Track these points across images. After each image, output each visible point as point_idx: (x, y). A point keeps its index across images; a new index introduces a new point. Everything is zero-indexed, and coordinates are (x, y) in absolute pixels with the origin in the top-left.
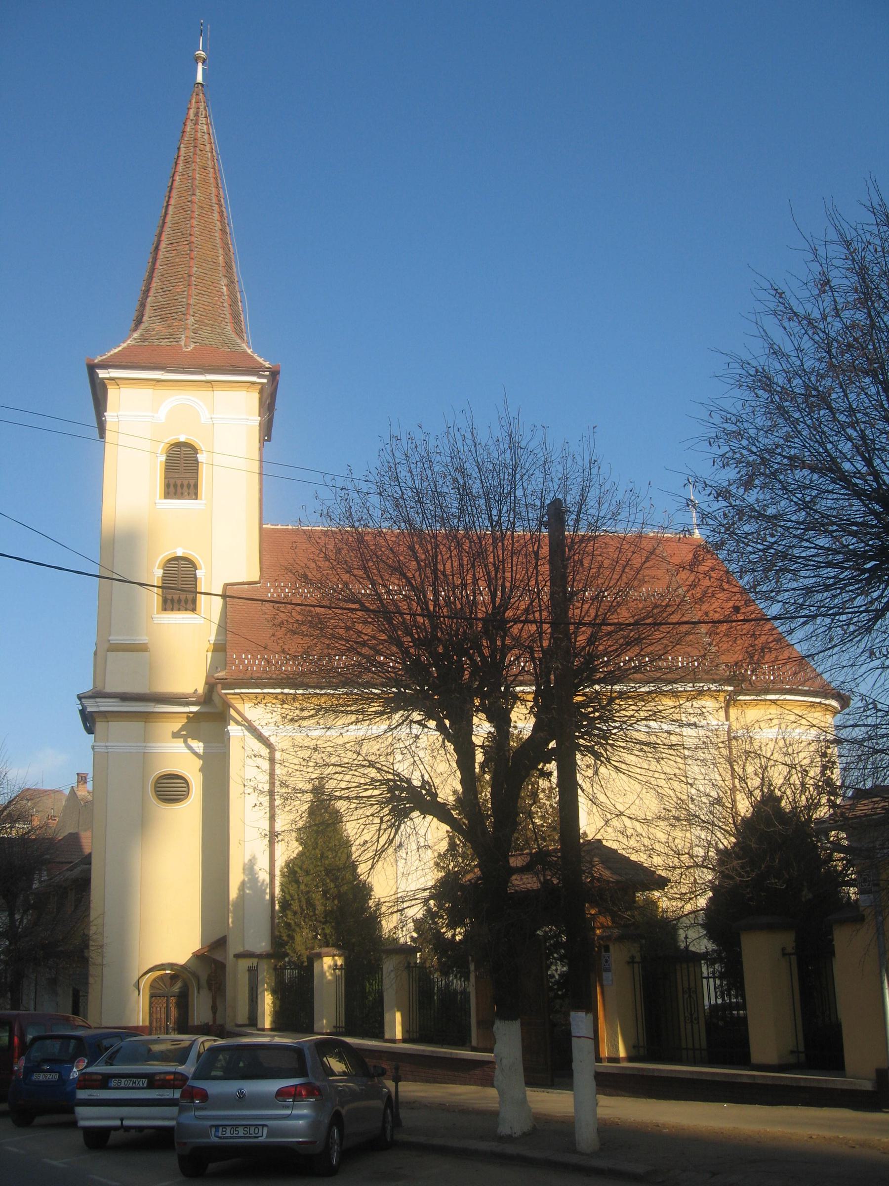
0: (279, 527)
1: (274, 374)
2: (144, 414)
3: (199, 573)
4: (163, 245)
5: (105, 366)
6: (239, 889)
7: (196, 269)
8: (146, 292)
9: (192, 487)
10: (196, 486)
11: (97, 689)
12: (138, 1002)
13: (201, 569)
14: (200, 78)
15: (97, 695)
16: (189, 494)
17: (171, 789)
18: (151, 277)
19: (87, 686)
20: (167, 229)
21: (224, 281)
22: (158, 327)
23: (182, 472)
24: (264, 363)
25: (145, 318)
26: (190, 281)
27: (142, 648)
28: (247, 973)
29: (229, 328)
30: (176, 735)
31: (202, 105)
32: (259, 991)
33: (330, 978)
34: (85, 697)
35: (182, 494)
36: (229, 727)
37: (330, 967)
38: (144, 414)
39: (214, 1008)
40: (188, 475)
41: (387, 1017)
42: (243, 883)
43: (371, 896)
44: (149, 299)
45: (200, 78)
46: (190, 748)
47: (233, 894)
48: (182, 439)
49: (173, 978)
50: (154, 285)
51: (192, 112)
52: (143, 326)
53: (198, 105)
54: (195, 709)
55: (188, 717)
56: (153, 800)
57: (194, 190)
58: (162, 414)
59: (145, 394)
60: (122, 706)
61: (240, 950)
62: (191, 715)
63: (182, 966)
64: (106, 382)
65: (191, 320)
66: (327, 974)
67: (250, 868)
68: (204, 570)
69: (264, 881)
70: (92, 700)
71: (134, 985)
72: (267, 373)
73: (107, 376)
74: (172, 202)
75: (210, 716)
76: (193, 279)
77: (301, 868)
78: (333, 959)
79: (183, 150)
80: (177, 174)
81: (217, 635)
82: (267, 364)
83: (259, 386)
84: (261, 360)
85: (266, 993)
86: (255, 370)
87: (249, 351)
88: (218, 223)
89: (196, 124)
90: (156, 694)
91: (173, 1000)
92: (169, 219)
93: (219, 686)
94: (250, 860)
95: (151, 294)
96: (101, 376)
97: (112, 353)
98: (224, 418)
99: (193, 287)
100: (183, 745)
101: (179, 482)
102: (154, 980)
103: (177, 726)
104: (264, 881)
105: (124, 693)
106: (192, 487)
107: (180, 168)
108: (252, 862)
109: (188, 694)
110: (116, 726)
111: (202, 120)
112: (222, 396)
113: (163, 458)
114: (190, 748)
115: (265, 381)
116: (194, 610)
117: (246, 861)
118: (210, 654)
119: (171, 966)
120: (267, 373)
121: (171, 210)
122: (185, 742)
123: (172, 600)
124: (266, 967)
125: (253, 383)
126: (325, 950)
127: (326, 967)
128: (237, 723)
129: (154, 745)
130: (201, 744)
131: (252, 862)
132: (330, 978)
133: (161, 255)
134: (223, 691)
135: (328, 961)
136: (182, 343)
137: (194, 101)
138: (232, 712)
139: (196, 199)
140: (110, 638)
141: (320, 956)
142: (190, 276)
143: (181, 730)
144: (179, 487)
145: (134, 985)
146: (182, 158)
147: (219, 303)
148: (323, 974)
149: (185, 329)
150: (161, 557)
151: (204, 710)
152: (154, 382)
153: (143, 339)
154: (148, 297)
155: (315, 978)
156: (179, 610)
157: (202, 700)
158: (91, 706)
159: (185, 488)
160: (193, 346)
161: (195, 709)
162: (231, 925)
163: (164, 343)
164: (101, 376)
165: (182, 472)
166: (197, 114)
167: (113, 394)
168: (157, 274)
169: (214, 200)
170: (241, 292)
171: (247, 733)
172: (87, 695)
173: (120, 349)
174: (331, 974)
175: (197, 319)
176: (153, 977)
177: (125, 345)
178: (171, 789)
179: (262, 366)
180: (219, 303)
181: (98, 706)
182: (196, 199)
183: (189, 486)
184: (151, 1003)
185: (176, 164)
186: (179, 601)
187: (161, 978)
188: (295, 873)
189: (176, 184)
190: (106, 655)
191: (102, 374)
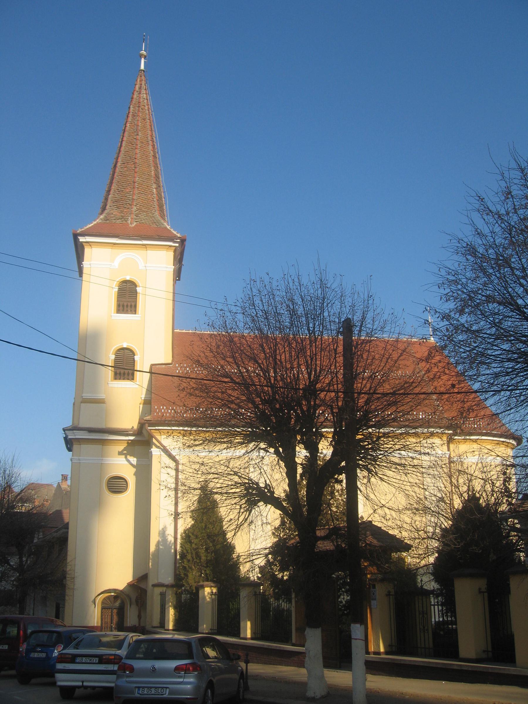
0: (184, 331)
1: (183, 241)
2: (105, 263)
3: (136, 358)
4: (119, 164)
5: (83, 234)
6: (156, 546)
7: (138, 178)
14: (142, 67)
15: (74, 428)
16: (131, 311)
17: (117, 485)
18: (111, 183)
19: (69, 423)
20: (122, 155)
21: (154, 186)
22: (116, 212)
23: (127, 297)
25: (108, 207)
26: (134, 185)
27: (101, 401)
28: (159, 596)
29: (157, 214)
30: (120, 453)
33: (208, 600)
34: (67, 430)
35: (127, 311)
36: (152, 449)
37: (208, 593)
38: (105, 263)
39: (139, 617)
40: (130, 300)
41: (242, 624)
42: (158, 542)
44: (110, 196)
45: (142, 67)
46: (128, 461)
47: (152, 548)
48: (128, 278)
49: (116, 598)
50: (113, 187)
52: (106, 211)
53: (141, 83)
54: (132, 438)
55: (128, 443)
57: (138, 132)
58: (116, 264)
61: (156, 582)
62: (130, 442)
64: (84, 244)
65: (135, 208)
66: (207, 598)
67: (163, 533)
68: (139, 356)
70: (71, 432)
72: (179, 240)
74: (125, 139)
75: (141, 442)
76: (136, 184)
77: (193, 534)
79: (132, 109)
80: (128, 122)
82: (179, 235)
83: (174, 248)
84: (175, 233)
85: (170, 608)
86: (171, 238)
87: (168, 227)
88: (152, 152)
89: (140, 93)
90: (109, 428)
91: (115, 611)
92: (123, 149)
93: (147, 425)
94: (163, 529)
95: (112, 192)
96: (81, 240)
97: (88, 227)
99: (136, 189)
100: (124, 459)
101: (125, 304)
102: (104, 599)
103: (121, 448)
104: (171, 541)
105: (90, 428)
107: (130, 119)
111: (143, 91)
112: (152, 254)
113: (116, 289)
115: (177, 245)
117: (161, 529)
118: (141, 406)
119: (115, 590)
120: (179, 240)
122: (126, 457)
123: (120, 374)
125: (170, 246)
126: (206, 583)
127: (206, 593)
128: (158, 447)
130: (135, 459)
132: (208, 600)
133: (117, 170)
135: (207, 590)
136: (129, 222)
137: (139, 80)
138: (154, 440)
139: (139, 137)
141: (203, 587)
142: (134, 182)
143: (125, 449)
144: (125, 307)
146: (131, 113)
148: (204, 597)
149: (131, 214)
152: (112, 245)
153: (106, 219)
157: (136, 433)
159: (129, 307)
160: (135, 224)
161: (132, 438)
162: (150, 567)
163: (118, 222)
164: (81, 240)
165: (127, 297)
166: (140, 88)
168: (115, 181)
170: (164, 192)
171: (162, 453)
172: (68, 428)
173: (92, 224)
174: (209, 598)
175: (138, 208)
177: (95, 222)
178: (117, 485)
181: (75, 435)
183: (131, 306)
184: (102, 612)
187: (108, 597)
188: (189, 537)
189: (127, 128)
191: (82, 239)
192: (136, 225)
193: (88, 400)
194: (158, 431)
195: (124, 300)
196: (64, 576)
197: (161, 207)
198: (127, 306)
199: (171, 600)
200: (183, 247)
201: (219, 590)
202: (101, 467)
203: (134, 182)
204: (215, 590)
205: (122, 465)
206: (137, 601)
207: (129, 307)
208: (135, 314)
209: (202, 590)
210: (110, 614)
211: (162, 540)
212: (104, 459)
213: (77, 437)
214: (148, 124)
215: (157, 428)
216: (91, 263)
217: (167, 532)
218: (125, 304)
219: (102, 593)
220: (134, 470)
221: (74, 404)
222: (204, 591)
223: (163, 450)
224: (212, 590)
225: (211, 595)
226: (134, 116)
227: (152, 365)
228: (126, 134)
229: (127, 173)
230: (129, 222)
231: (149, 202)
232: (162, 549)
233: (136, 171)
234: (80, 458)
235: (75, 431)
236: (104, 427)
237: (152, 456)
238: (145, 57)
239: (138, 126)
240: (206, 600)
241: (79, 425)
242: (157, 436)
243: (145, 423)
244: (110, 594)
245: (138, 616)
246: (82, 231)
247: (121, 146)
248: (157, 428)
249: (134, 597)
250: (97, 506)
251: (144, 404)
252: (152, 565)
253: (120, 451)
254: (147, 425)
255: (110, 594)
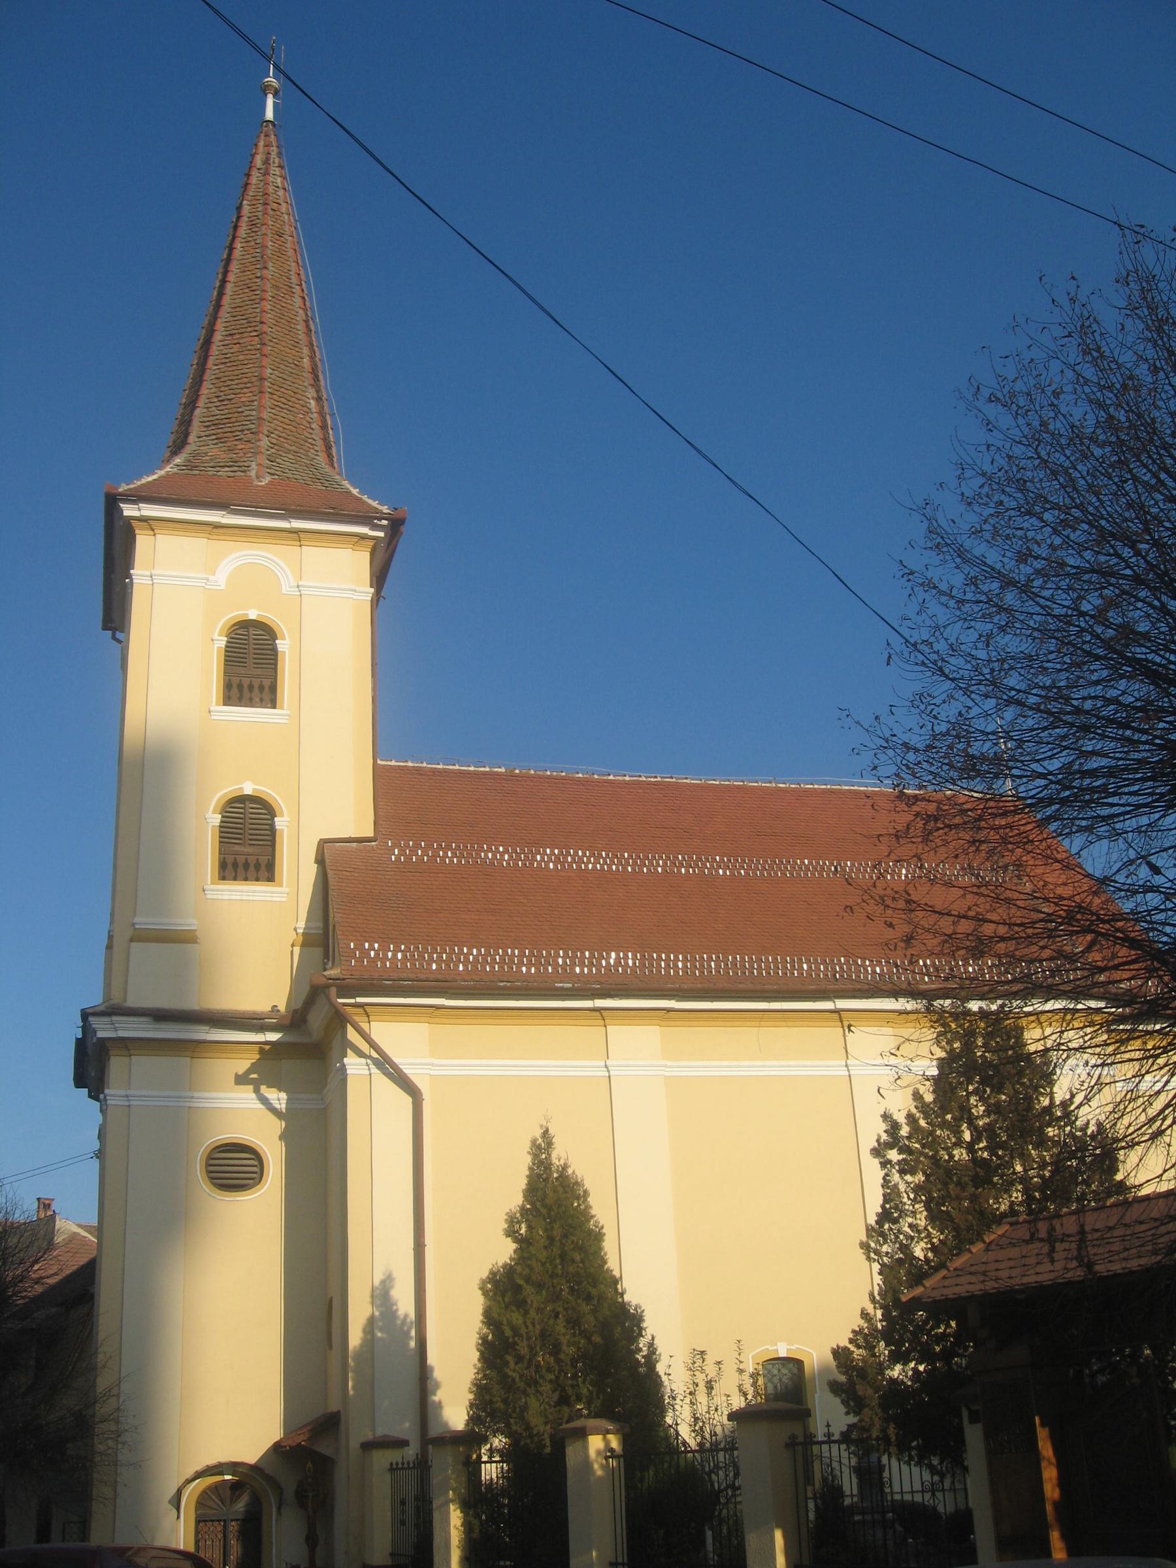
0: (393, 763)
1: (396, 526)
2: (192, 579)
3: (279, 822)
4: (218, 337)
5: (138, 497)
6: (364, 1331)
7: (269, 371)
8: (192, 404)
9: (267, 689)
10: (273, 689)
11: (113, 1002)
12: (176, 1531)
13: (282, 816)
14: (269, 114)
15: (113, 1011)
16: (261, 700)
17: (234, 1168)
18: (198, 381)
19: (95, 998)
20: (224, 314)
21: (311, 393)
22: (214, 451)
23: (251, 664)
24: (380, 508)
25: (192, 438)
26: (262, 386)
27: (187, 938)
28: (388, 1477)
29: (322, 459)
30: (241, 1080)
31: (274, 151)
32: (435, 1504)
33: (599, 1473)
34: (95, 1014)
35: (251, 699)
36: (346, 1060)
37: (599, 1453)
38: (192, 579)
39: (311, 1540)
40: (258, 672)
41: (752, 1541)
42: (371, 1321)
43: (641, 1329)
44: (197, 412)
45: (269, 114)
46: (264, 1101)
47: (355, 1338)
48: (253, 615)
49: (236, 1487)
50: (204, 391)
51: (258, 161)
52: (188, 449)
53: (266, 150)
54: (273, 1037)
55: (261, 1051)
56: (204, 1186)
57: (265, 262)
58: (221, 578)
59: (194, 546)
60: (156, 1030)
61: (369, 1436)
62: (267, 1047)
63: (254, 1468)
64: (134, 523)
65: (265, 442)
66: (596, 1466)
67: (382, 1295)
68: (286, 818)
69: (406, 1316)
70: (106, 1019)
71: (170, 1502)
72: (385, 522)
73: (136, 514)
74: (231, 277)
75: (307, 1047)
76: (267, 384)
77: (528, 1280)
78: (605, 1439)
79: (246, 209)
80: (238, 240)
81: (308, 920)
82: (385, 509)
83: (371, 543)
84: (375, 504)
85: (452, 1507)
86: (366, 517)
87: (355, 492)
88: (301, 312)
89: (266, 173)
90: (210, 1012)
91: (234, 1527)
92: (226, 300)
93: (333, 990)
94: (383, 1282)
95: (201, 402)
96: (126, 513)
97: (143, 481)
98: (321, 591)
99: (268, 395)
100: (254, 1096)
101: (246, 682)
102: (204, 1492)
103: (243, 1064)
104: (406, 1316)
105: (158, 1010)
106: (267, 689)
107: (243, 231)
108: (388, 1282)
109: (262, 1013)
110: (142, 1064)
111: (274, 170)
112: (315, 555)
113: (222, 642)
114: (264, 1101)
115: (382, 534)
116: (271, 878)
117: (377, 1282)
118: (297, 950)
119: (234, 1467)
120: (385, 522)
121: (229, 288)
122: (257, 1091)
123: (235, 865)
124: (450, 1459)
125: (363, 537)
126: (591, 1423)
127: (592, 1453)
128: (360, 1054)
129: (214, 1095)
130: (283, 1095)
131: (388, 1282)
132: (599, 1473)
133: (215, 350)
134: (340, 1001)
135: (595, 1443)
136: (253, 474)
137: (261, 144)
138: (352, 1035)
139: (267, 274)
140: (136, 920)
141: (582, 1434)
142: (262, 379)
143: (253, 1068)
144: (246, 690)
145: (170, 1502)
146: (245, 219)
147: (305, 423)
148: (587, 1464)
149: (256, 454)
150: (222, 793)
151: (291, 1039)
152: (209, 528)
153: (190, 465)
154: (194, 408)
155: (570, 1475)
156: (246, 879)
157: (288, 1022)
158: (104, 1030)
159: (256, 690)
160: (268, 478)
161: (273, 1037)
162: (351, 1392)
163: (224, 472)
164: (126, 513)
165: (251, 664)
166: (266, 162)
167: (143, 541)
168: (208, 375)
169: (294, 279)
170: (332, 415)
171: (374, 1070)
172: (97, 1009)
173: (155, 477)
174: (602, 1466)
175: (274, 441)
176: (201, 1488)
177: (162, 473)
178: (234, 1168)
179: (377, 511)
180: (305, 423)
181: (116, 1030)
182: (267, 274)
183: (261, 688)
184: (197, 1532)
185: (236, 227)
186: (246, 866)
187: (215, 1489)
188: (518, 1289)
189: (237, 253)
190: (129, 947)
191: (129, 510)
192: (271, 483)
193: (147, 933)
194: (360, 1010)
195: (242, 671)
196: (83, 1425)
197: (328, 447)
198: (251, 687)
199: (453, 1483)
200: (391, 547)
201: (625, 1441)
202: (178, 1119)
203: (262, 379)
204: (615, 1442)
205: (242, 1109)
206: (301, 1497)
207: (256, 690)
208: (274, 707)
209: (579, 1444)
210: (220, 1536)
211: (381, 1313)
212: (196, 1094)
213: (121, 1034)
214: (288, 245)
215: (360, 1000)
216: (154, 572)
217: (395, 1293)
218: (246, 682)
219: (198, 1475)
220: (278, 1126)
221: (109, 947)
222: (586, 1447)
223: (377, 1063)
224: (607, 1442)
225: (607, 1458)
226: (252, 224)
227: (323, 843)
228: (234, 267)
229: (241, 357)
230: (253, 474)
231: (300, 431)
232: (380, 1339)
233: (265, 352)
234: (130, 1092)
235: (114, 1018)
236: (196, 1008)
237: (344, 1081)
238: (276, 94)
239: (265, 247)
240: (594, 1472)
241: (125, 1001)
242: (357, 1019)
243: (328, 986)
244: (218, 1478)
245: (308, 1539)
246: (130, 490)
247: (221, 294)
248: (360, 1000)
249: (290, 1485)
250: (172, 1221)
251: (304, 945)
252: (354, 1388)
253: (240, 1073)
254: (333, 990)
255: (218, 1478)
